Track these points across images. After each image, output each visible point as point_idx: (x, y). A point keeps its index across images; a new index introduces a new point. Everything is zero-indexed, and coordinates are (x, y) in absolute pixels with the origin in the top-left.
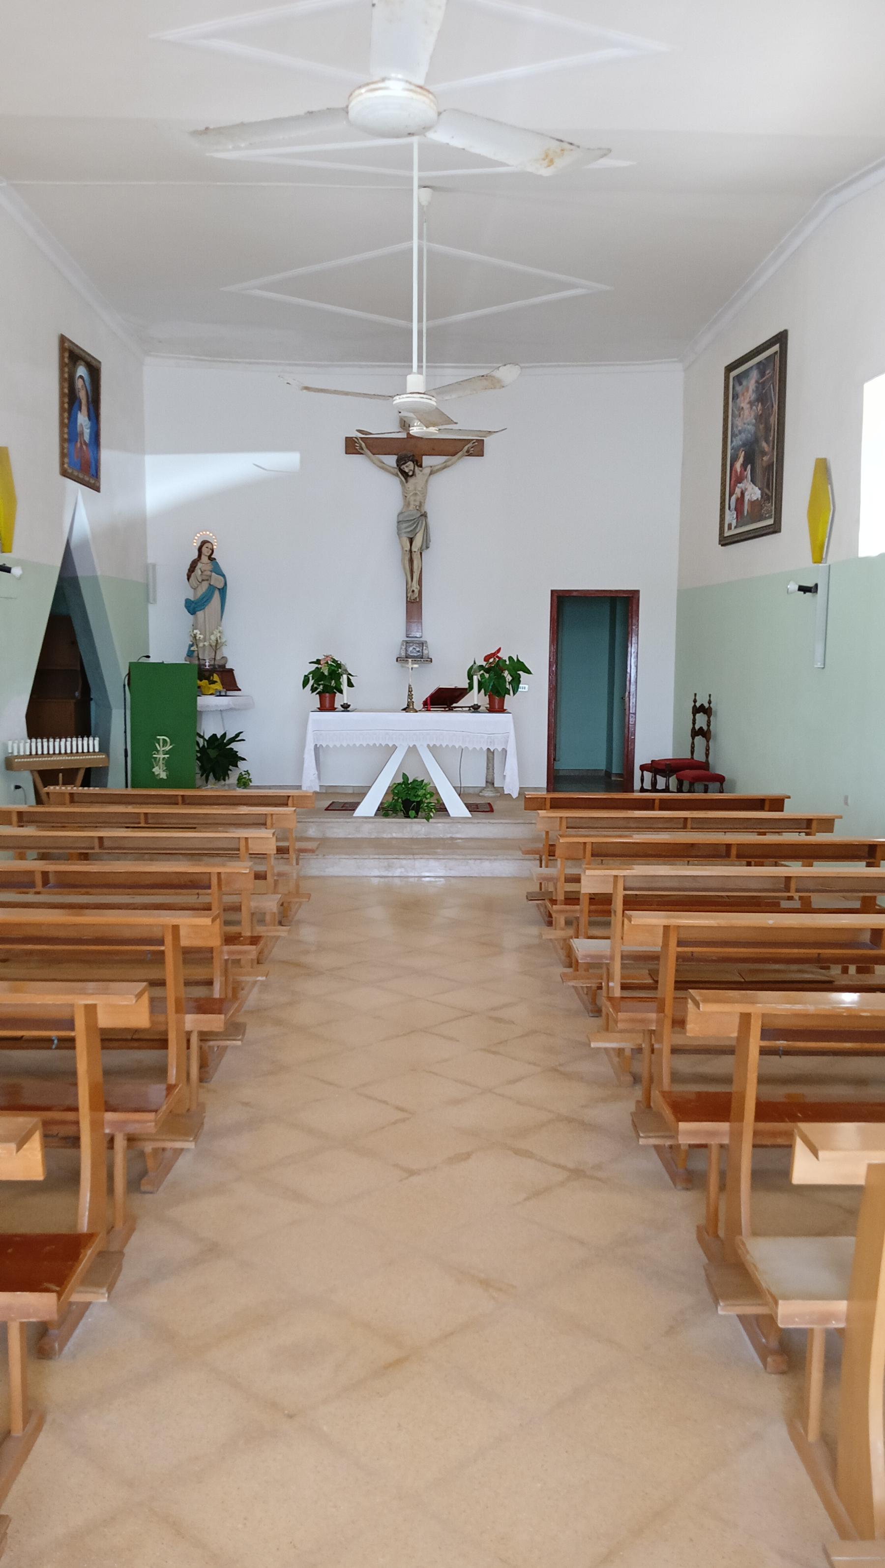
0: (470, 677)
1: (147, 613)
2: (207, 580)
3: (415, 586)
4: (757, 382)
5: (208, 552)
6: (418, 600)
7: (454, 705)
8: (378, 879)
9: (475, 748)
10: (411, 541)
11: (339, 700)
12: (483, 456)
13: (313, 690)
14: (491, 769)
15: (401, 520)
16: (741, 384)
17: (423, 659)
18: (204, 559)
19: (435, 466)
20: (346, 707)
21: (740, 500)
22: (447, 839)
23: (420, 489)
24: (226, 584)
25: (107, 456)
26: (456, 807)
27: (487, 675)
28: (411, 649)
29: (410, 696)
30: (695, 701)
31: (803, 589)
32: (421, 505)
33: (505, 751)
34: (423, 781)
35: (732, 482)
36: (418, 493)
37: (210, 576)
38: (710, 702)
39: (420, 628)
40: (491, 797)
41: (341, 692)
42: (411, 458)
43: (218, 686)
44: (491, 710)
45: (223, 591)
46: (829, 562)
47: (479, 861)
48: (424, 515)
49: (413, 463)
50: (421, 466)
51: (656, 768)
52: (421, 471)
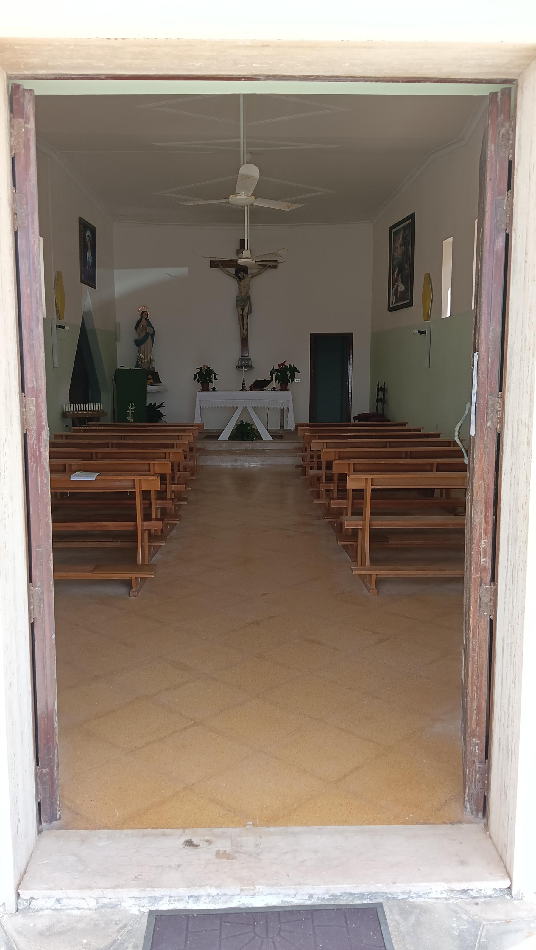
0: (272, 375)
1: (116, 345)
2: (145, 330)
4: (403, 235)
5: (145, 317)
7: (264, 388)
8: (230, 466)
9: (274, 408)
10: (243, 310)
11: (211, 386)
13: (198, 381)
14: (282, 420)
16: (396, 236)
17: (250, 367)
18: (144, 320)
19: (254, 274)
20: (214, 389)
21: (397, 290)
22: (262, 450)
24: (154, 331)
25: (99, 272)
26: (266, 436)
27: (279, 374)
28: (243, 362)
29: (244, 383)
30: (378, 385)
31: (420, 332)
32: (247, 293)
33: (288, 409)
34: (250, 423)
35: (393, 281)
37: (147, 328)
38: (384, 385)
39: (247, 352)
40: (283, 433)
41: (212, 382)
43: (152, 381)
44: (281, 390)
45: (153, 335)
46: (431, 320)
47: (276, 457)
48: (249, 297)
50: (247, 274)
51: (361, 417)
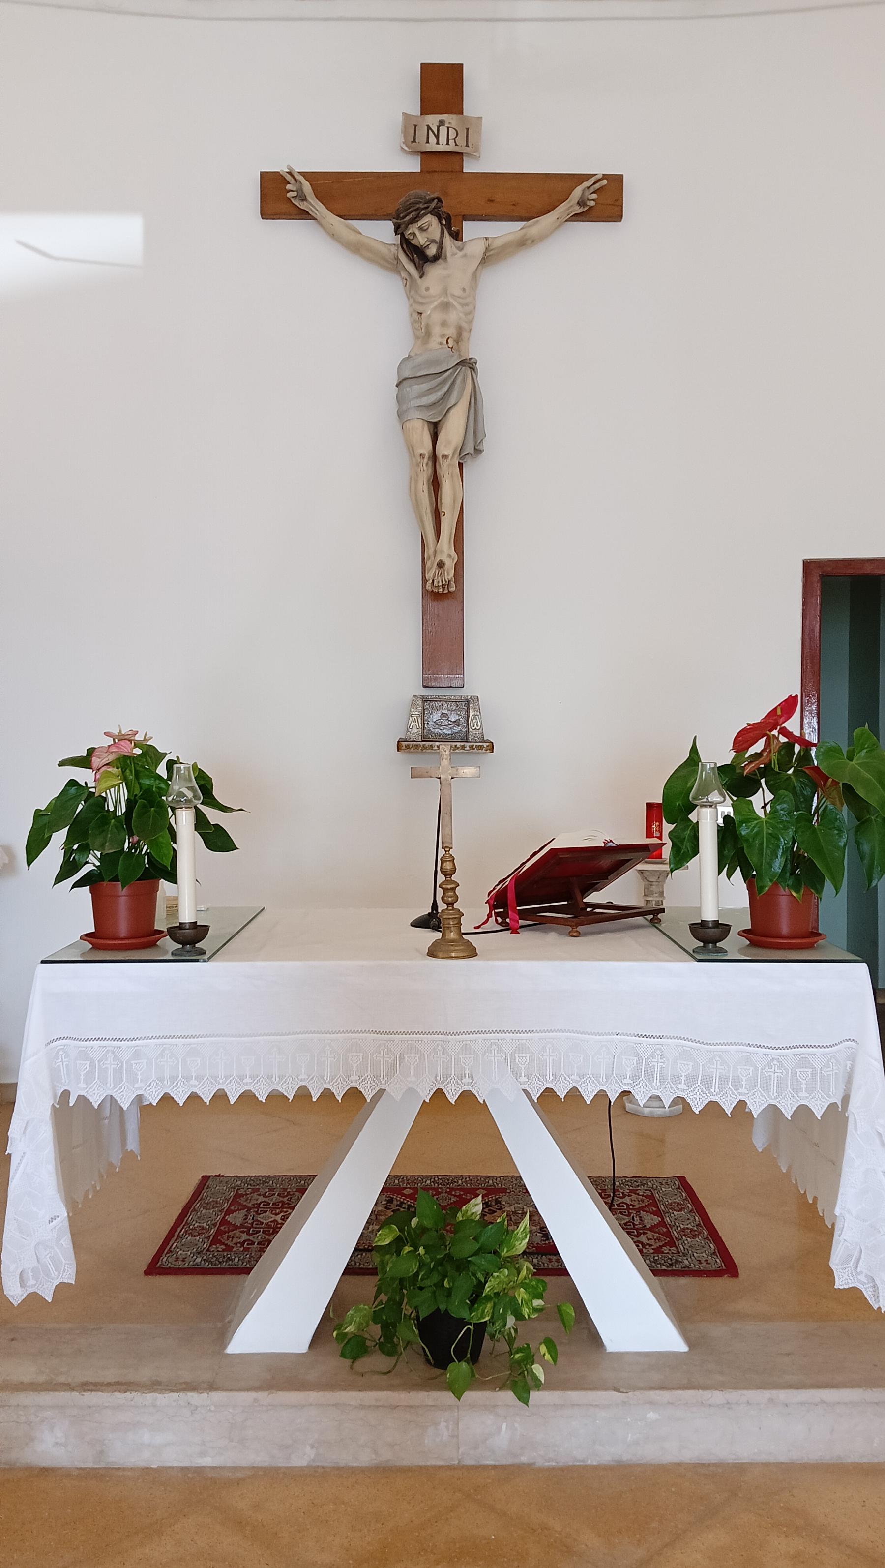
3: (445, 549)
6: (453, 589)
10: (435, 429)
12: (617, 216)
15: (407, 374)
23: (458, 292)
28: (436, 716)
36: (451, 300)
42: (433, 205)
49: (440, 220)
52: (461, 249)
